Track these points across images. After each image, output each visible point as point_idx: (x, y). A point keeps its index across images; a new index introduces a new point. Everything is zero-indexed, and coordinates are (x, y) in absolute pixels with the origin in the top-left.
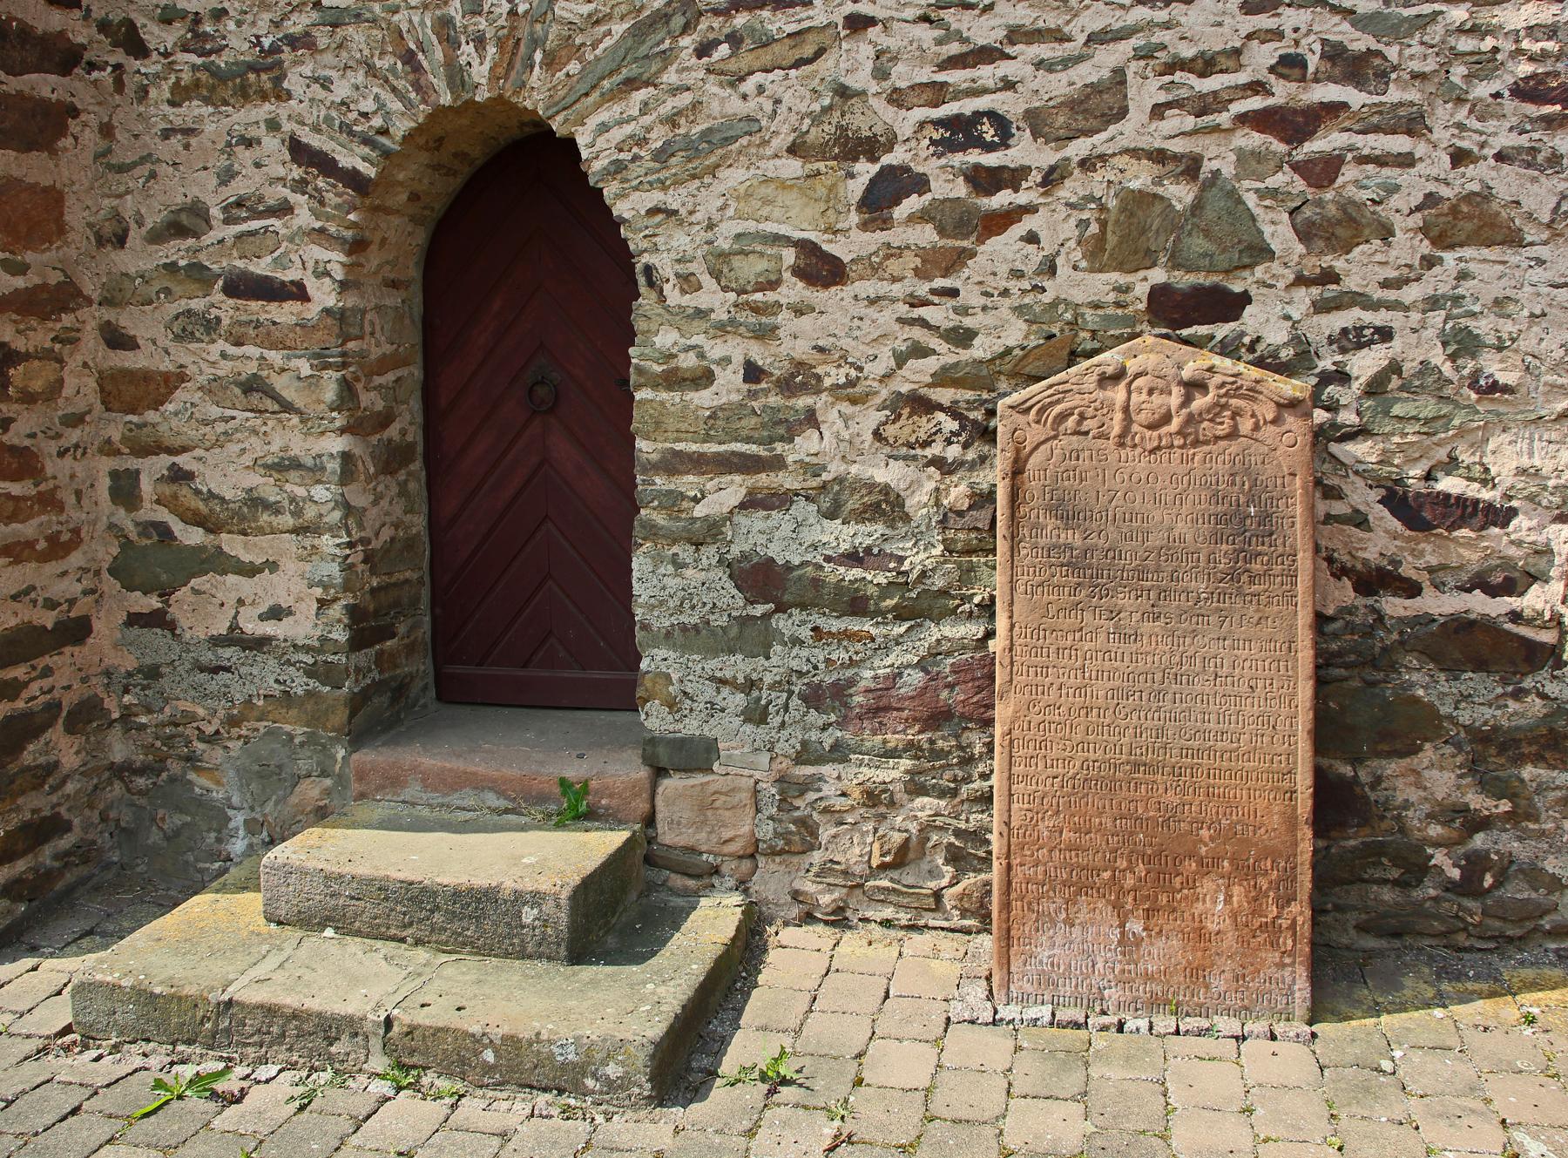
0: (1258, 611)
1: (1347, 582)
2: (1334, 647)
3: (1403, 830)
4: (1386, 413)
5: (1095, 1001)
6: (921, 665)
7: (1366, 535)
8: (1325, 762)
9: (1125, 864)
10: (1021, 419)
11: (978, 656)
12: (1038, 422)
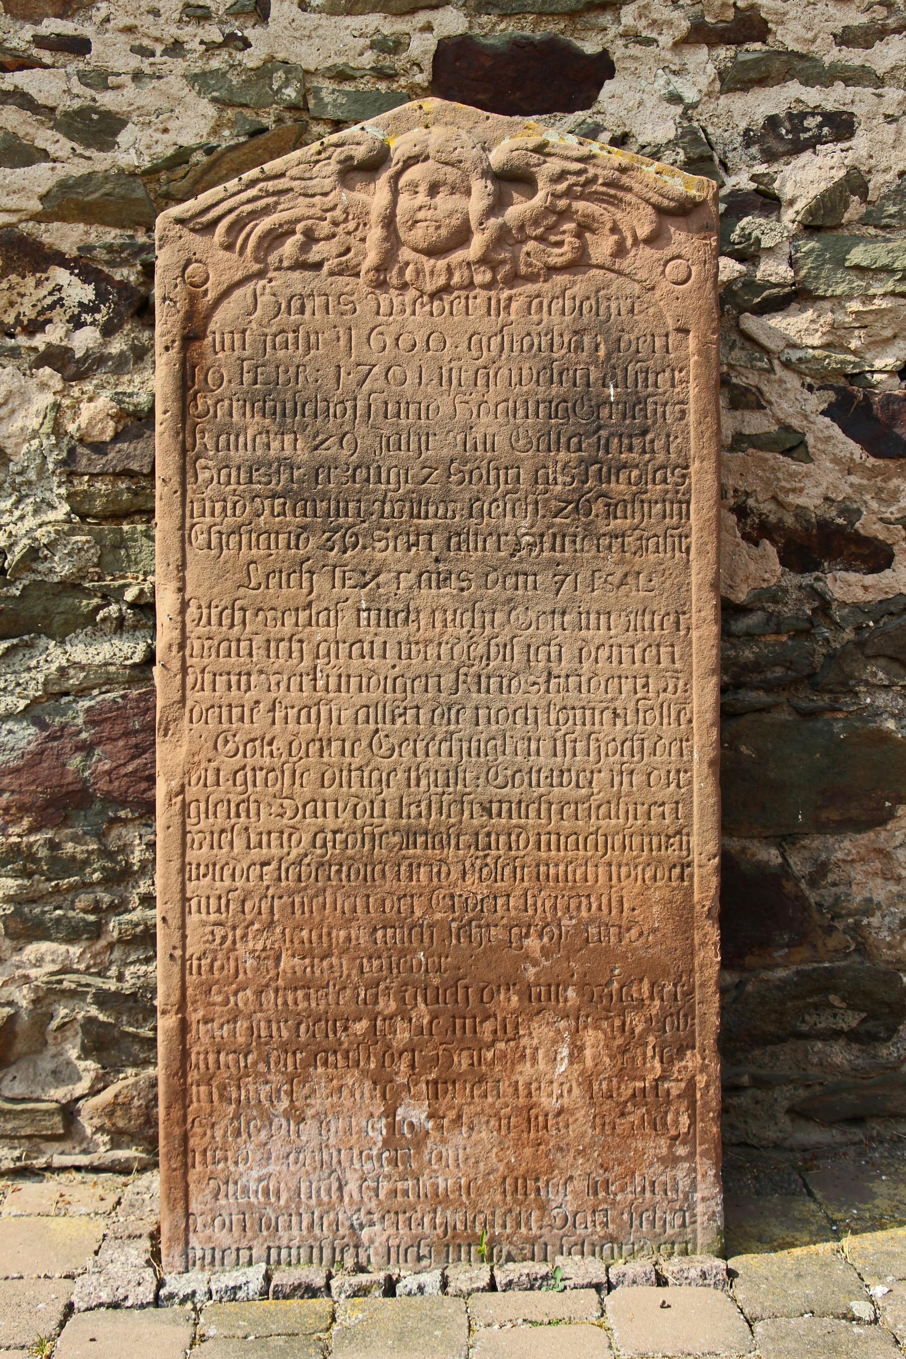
0: (621, 562)
1: (769, 548)
2: (748, 654)
3: (863, 949)
4: (839, 262)
5: (346, 1250)
6: (31, 713)
7: (803, 468)
8: (735, 844)
9: (393, 1005)
10: (197, 242)
11: (134, 693)
12: (229, 247)
